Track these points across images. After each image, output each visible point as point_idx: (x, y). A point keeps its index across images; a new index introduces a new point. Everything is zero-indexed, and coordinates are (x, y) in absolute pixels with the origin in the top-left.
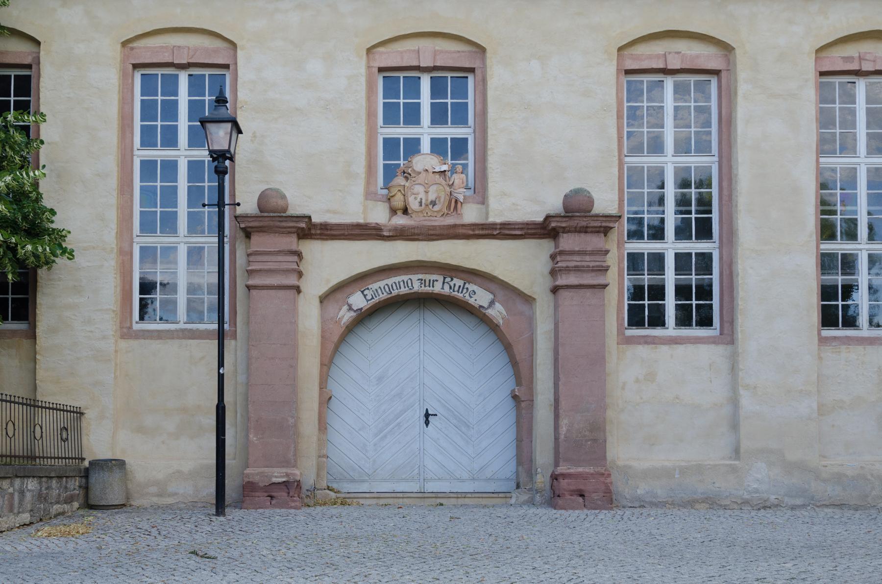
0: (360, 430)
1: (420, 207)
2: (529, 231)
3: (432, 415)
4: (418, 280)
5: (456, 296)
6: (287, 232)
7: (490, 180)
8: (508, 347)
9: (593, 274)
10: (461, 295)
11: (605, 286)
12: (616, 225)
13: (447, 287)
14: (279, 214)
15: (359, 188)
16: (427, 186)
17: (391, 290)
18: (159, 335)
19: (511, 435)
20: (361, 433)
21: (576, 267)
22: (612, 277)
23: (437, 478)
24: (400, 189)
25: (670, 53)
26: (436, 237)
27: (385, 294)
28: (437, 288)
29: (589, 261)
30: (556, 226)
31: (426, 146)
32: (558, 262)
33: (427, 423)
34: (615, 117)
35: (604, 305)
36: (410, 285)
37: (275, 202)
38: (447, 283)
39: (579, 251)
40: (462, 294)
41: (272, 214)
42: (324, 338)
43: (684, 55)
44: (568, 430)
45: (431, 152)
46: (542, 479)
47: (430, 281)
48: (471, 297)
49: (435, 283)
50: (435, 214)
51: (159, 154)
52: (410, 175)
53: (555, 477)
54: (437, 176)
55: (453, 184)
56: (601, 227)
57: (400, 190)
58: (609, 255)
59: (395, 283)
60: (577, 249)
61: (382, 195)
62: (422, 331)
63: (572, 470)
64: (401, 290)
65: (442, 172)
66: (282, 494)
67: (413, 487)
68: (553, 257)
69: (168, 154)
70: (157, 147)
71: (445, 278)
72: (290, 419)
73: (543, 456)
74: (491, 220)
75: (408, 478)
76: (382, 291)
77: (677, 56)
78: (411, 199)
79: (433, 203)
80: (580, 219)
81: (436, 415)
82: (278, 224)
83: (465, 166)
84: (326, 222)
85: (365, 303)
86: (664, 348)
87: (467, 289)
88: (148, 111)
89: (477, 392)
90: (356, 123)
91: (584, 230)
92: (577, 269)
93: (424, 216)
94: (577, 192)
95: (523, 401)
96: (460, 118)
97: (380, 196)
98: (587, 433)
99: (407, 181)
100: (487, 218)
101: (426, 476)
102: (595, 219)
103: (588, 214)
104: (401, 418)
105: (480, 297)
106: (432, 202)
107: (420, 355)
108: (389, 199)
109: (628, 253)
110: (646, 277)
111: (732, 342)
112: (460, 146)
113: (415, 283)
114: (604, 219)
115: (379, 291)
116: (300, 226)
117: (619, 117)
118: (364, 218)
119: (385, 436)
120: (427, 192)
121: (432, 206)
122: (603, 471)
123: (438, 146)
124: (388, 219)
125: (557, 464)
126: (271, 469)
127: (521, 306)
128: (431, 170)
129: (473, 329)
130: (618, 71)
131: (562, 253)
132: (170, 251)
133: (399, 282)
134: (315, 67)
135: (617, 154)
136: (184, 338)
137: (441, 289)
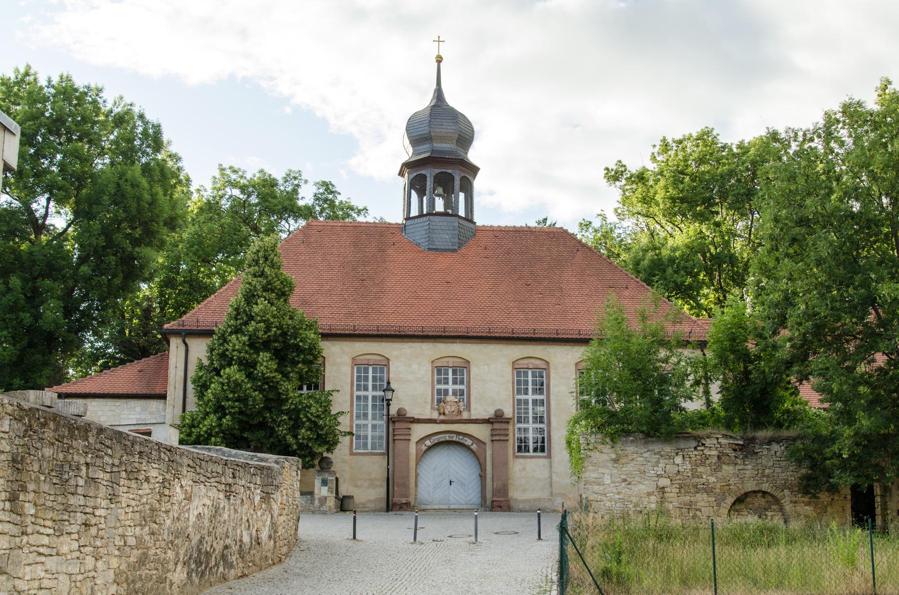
6: (407, 422)
8: (478, 459)
15: (429, 407)
16: (451, 406)
18: (363, 454)
19: (479, 489)
28: (454, 439)
29: (502, 432)
31: (450, 392)
37: (403, 413)
46: (488, 503)
51: (362, 393)
53: (492, 502)
66: (405, 507)
67: (446, 507)
69: (365, 393)
73: (489, 495)
74: (472, 418)
83: (463, 399)
88: (359, 378)
91: (501, 422)
92: (499, 435)
94: (499, 410)
96: (462, 383)
105: (468, 442)
111: (550, 458)
112: (462, 393)
113: (447, 437)
117: (513, 383)
123: (455, 393)
127: (482, 445)
132: (365, 426)
134: (415, 367)
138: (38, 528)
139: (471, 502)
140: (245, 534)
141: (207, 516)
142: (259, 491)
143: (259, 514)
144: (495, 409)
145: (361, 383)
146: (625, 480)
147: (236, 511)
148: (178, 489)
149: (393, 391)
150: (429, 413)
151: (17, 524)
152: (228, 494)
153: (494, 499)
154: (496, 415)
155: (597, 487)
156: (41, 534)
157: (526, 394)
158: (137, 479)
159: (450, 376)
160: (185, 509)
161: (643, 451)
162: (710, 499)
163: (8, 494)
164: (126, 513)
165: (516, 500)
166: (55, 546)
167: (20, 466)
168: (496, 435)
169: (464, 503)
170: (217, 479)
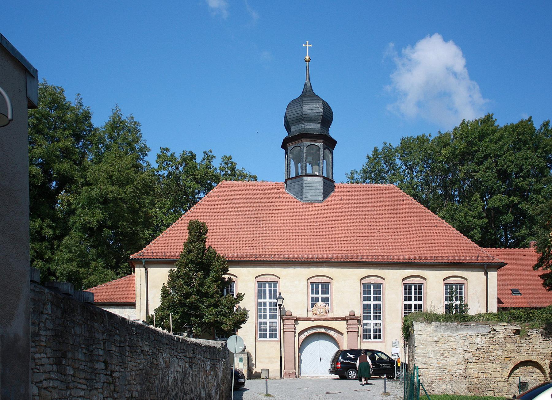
18: (264, 341)
31: (320, 300)
78: (317, 312)
86: (371, 344)
92: (352, 328)
105: (332, 333)
123: (323, 300)
137: (31, 346)
138: (76, 384)
140: (202, 391)
141: (179, 379)
142: (209, 363)
143: (210, 378)
145: (261, 294)
146: (442, 355)
147: (196, 375)
148: (161, 361)
149: (283, 299)
151: (62, 382)
152: (191, 364)
155: (425, 359)
156: (78, 388)
157: (370, 300)
158: (135, 352)
159: (320, 289)
160: (166, 374)
161: (455, 335)
162: (498, 366)
163: (54, 359)
164: (131, 375)
166: (88, 397)
167: (61, 340)
168: (350, 328)
170: (184, 354)
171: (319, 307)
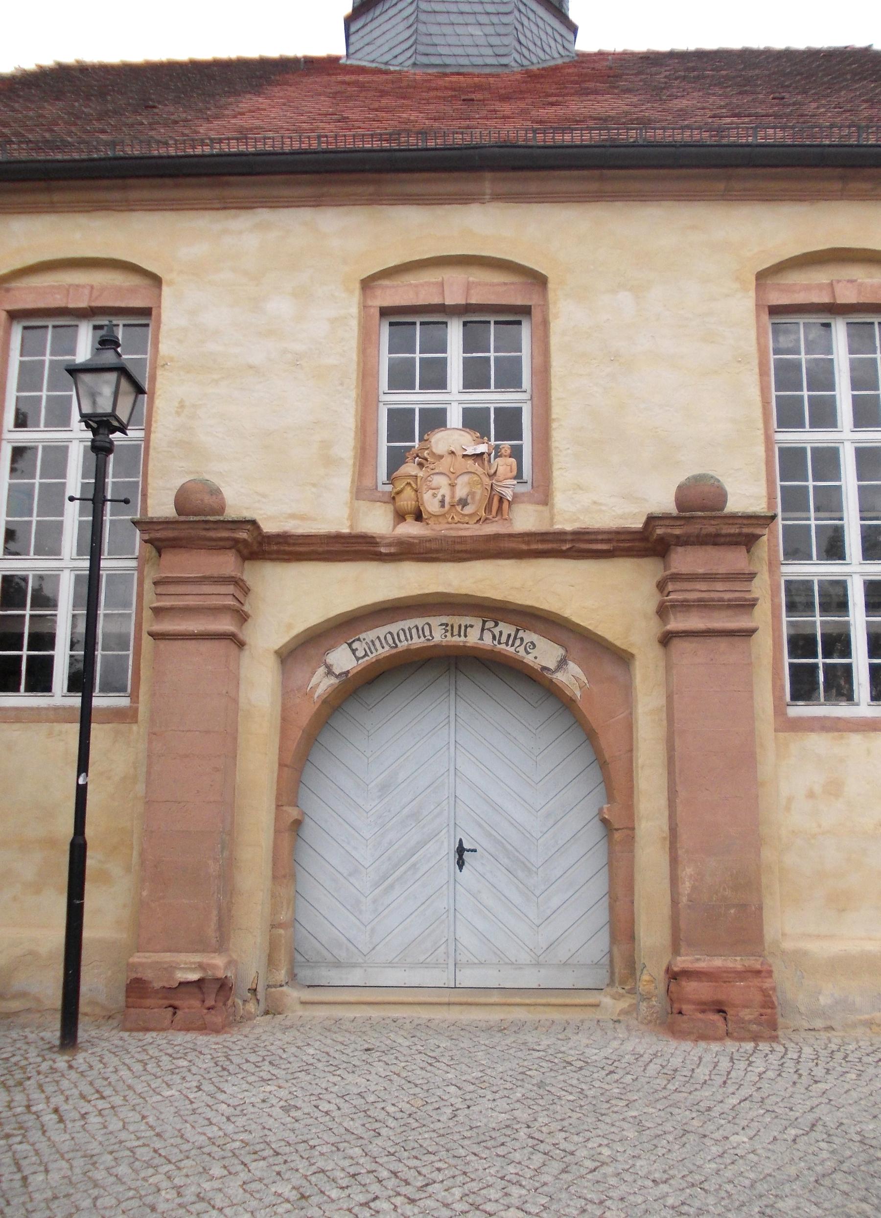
0: (350, 875)
1: (442, 509)
2: (622, 545)
3: (468, 851)
4: (441, 625)
5: (503, 652)
7: (555, 467)
9: (730, 612)
10: (512, 649)
11: (749, 633)
12: (766, 531)
13: (488, 637)
14: (203, 518)
17: (397, 641)
19: (599, 886)
20: (352, 880)
21: (700, 600)
22: (761, 617)
23: (476, 961)
24: (409, 481)
25: (839, 281)
26: (468, 556)
27: (387, 648)
28: (473, 638)
29: (722, 591)
30: (665, 534)
31: (455, 418)
32: (669, 592)
33: (461, 863)
34: (757, 370)
35: (750, 664)
36: (427, 633)
38: (489, 629)
39: (704, 574)
40: (513, 648)
41: (192, 518)
42: (285, 720)
43: (861, 285)
44: (694, 888)
45: (463, 426)
47: (460, 626)
48: (528, 653)
49: (469, 629)
50: (467, 519)
52: (426, 460)
53: (674, 976)
54: (470, 462)
55: (495, 472)
56: (740, 534)
57: (409, 484)
58: (756, 581)
59: (403, 630)
60: (701, 571)
61: (383, 492)
62: (453, 708)
63: (704, 964)
64: (414, 641)
65: (477, 455)
66: (190, 1005)
68: (661, 586)
70: (38, 426)
71: (484, 622)
72: (210, 862)
74: (558, 527)
75: (428, 960)
76: (381, 643)
77: (849, 285)
78: (427, 496)
79: (464, 503)
80: (705, 522)
81: (475, 851)
82: (203, 533)
84: (286, 533)
85: (354, 663)
86: (856, 739)
87: (522, 639)
89: (542, 810)
90: (342, 384)
91: (714, 540)
92: (703, 605)
93: (448, 523)
94: (698, 480)
95: (617, 830)
97: (380, 494)
98: (728, 893)
99: (421, 469)
100: (552, 524)
101: (459, 957)
102: (731, 521)
103: (718, 513)
104: (419, 853)
106: (460, 500)
107: (449, 748)
108: (394, 498)
109: (786, 581)
110: (818, 619)
114: (745, 522)
115: (377, 643)
116: (238, 536)
117: (763, 373)
118: (351, 527)
119: (391, 887)
120: (452, 486)
121: (460, 507)
122: (758, 966)
124: (391, 528)
125: (676, 950)
126: (175, 954)
127: (610, 668)
128: (460, 453)
129: (536, 705)
130: (758, 306)
131: (676, 577)
133: (410, 629)
135: (761, 425)
136: (58, 721)
139: (562, 953)
144: (681, 477)
150: (345, 512)
153: (683, 962)
154: (680, 504)
165: (798, 959)
169: (524, 957)
171: (445, 465)
